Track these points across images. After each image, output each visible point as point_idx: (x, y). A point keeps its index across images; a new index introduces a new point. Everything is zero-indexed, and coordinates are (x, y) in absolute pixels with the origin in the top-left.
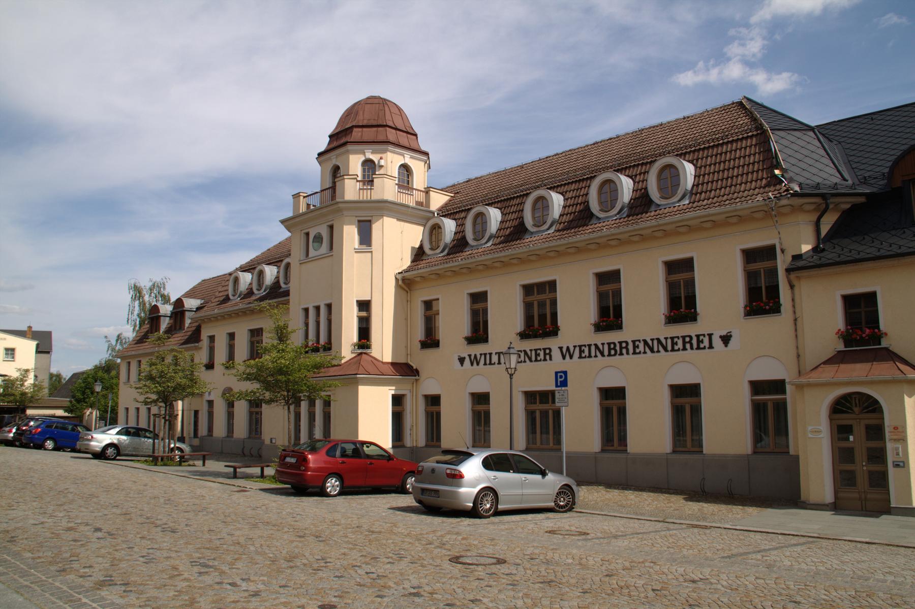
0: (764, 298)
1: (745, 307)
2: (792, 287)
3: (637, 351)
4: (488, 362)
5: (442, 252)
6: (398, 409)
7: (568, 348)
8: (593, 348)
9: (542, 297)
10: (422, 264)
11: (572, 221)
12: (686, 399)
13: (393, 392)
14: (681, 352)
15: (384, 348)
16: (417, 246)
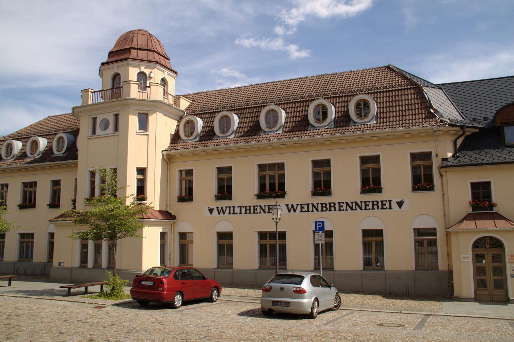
0: (225, 192)
1: (312, 192)
2: (441, 176)
3: (256, 212)
4: (232, 212)
5: (194, 139)
6: (52, 241)
7: (292, 206)
8: (310, 206)
9: (31, 189)
10: (180, 146)
11: (294, 127)
12: (373, 239)
13: (161, 231)
14: (371, 210)
15: (154, 198)
16: (173, 133)
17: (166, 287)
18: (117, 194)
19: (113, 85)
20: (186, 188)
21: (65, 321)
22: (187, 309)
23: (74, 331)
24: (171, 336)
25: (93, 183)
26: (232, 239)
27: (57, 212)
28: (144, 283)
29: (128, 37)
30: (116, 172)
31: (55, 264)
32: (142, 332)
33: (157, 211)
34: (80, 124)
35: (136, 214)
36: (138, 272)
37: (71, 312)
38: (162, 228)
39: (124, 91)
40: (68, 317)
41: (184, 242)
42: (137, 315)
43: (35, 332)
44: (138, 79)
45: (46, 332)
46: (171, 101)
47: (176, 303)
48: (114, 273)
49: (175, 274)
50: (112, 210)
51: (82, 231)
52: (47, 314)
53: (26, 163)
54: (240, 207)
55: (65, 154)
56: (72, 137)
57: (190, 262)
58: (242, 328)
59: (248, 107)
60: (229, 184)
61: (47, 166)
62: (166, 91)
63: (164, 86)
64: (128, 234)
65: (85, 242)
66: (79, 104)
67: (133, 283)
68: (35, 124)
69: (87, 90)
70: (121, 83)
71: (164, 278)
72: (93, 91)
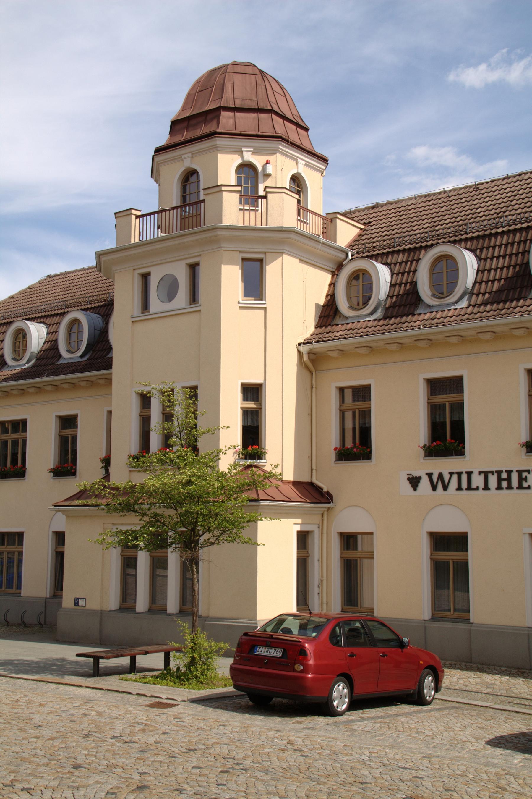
3: (525, 485)
4: (464, 485)
5: (372, 313)
6: (60, 550)
9: (15, 436)
10: (339, 331)
13: (298, 528)
15: (281, 454)
17: (311, 662)
18: (200, 445)
19: (184, 198)
20: (354, 429)
21: (87, 736)
22: (362, 719)
23: (105, 762)
24: (325, 789)
25: (145, 421)
26: (466, 550)
27: (70, 486)
28: (261, 651)
29: (212, 82)
30: (196, 396)
31: (67, 602)
32: (258, 774)
33: (288, 482)
34: (115, 290)
35: (241, 489)
36: (247, 623)
37: (100, 714)
38: (299, 521)
39: (207, 209)
40: (92, 728)
41: (351, 554)
42: (246, 728)
43: (23, 760)
44: (239, 179)
45: (45, 761)
46: (314, 226)
47: (335, 704)
48: (193, 626)
49: (333, 631)
50: (189, 483)
51: (124, 528)
52: (49, 718)
53: (5, 380)
54: (486, 474)
55: (85, 358)
56: (97, 318)
57: (366, 604)
58: (503, 782)
59: (500, 230)
60: (456, 418)
61: (47, 384)
62: (302, 204)
63: (298, 193)
64: (225, 536)
65: (129, 553)
66: (110, 244)
67: (237, 650)
68: (20, 293)
69: (127, 212)
70: (202, 191)
71: (307, 641)
72: (139, 213)
